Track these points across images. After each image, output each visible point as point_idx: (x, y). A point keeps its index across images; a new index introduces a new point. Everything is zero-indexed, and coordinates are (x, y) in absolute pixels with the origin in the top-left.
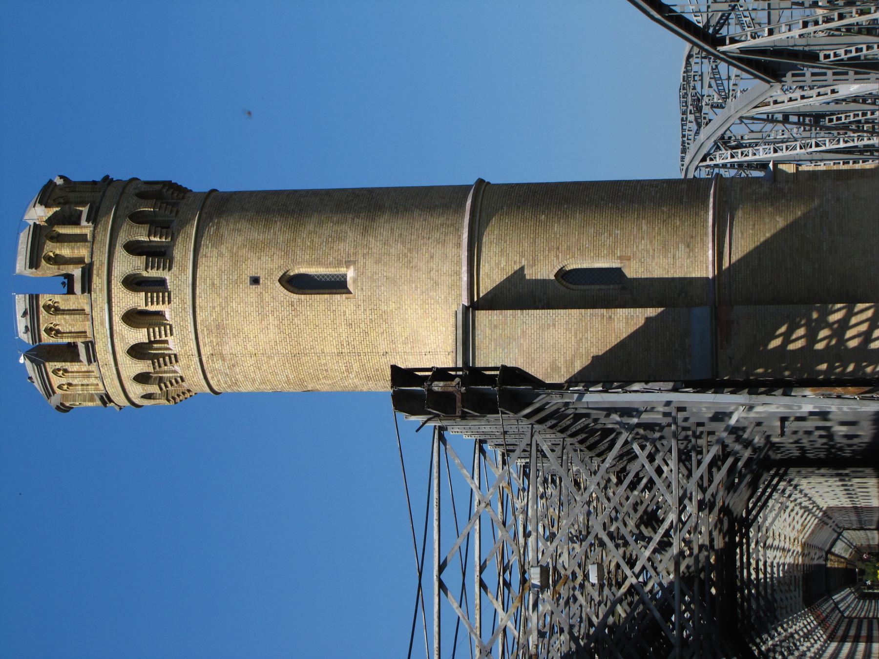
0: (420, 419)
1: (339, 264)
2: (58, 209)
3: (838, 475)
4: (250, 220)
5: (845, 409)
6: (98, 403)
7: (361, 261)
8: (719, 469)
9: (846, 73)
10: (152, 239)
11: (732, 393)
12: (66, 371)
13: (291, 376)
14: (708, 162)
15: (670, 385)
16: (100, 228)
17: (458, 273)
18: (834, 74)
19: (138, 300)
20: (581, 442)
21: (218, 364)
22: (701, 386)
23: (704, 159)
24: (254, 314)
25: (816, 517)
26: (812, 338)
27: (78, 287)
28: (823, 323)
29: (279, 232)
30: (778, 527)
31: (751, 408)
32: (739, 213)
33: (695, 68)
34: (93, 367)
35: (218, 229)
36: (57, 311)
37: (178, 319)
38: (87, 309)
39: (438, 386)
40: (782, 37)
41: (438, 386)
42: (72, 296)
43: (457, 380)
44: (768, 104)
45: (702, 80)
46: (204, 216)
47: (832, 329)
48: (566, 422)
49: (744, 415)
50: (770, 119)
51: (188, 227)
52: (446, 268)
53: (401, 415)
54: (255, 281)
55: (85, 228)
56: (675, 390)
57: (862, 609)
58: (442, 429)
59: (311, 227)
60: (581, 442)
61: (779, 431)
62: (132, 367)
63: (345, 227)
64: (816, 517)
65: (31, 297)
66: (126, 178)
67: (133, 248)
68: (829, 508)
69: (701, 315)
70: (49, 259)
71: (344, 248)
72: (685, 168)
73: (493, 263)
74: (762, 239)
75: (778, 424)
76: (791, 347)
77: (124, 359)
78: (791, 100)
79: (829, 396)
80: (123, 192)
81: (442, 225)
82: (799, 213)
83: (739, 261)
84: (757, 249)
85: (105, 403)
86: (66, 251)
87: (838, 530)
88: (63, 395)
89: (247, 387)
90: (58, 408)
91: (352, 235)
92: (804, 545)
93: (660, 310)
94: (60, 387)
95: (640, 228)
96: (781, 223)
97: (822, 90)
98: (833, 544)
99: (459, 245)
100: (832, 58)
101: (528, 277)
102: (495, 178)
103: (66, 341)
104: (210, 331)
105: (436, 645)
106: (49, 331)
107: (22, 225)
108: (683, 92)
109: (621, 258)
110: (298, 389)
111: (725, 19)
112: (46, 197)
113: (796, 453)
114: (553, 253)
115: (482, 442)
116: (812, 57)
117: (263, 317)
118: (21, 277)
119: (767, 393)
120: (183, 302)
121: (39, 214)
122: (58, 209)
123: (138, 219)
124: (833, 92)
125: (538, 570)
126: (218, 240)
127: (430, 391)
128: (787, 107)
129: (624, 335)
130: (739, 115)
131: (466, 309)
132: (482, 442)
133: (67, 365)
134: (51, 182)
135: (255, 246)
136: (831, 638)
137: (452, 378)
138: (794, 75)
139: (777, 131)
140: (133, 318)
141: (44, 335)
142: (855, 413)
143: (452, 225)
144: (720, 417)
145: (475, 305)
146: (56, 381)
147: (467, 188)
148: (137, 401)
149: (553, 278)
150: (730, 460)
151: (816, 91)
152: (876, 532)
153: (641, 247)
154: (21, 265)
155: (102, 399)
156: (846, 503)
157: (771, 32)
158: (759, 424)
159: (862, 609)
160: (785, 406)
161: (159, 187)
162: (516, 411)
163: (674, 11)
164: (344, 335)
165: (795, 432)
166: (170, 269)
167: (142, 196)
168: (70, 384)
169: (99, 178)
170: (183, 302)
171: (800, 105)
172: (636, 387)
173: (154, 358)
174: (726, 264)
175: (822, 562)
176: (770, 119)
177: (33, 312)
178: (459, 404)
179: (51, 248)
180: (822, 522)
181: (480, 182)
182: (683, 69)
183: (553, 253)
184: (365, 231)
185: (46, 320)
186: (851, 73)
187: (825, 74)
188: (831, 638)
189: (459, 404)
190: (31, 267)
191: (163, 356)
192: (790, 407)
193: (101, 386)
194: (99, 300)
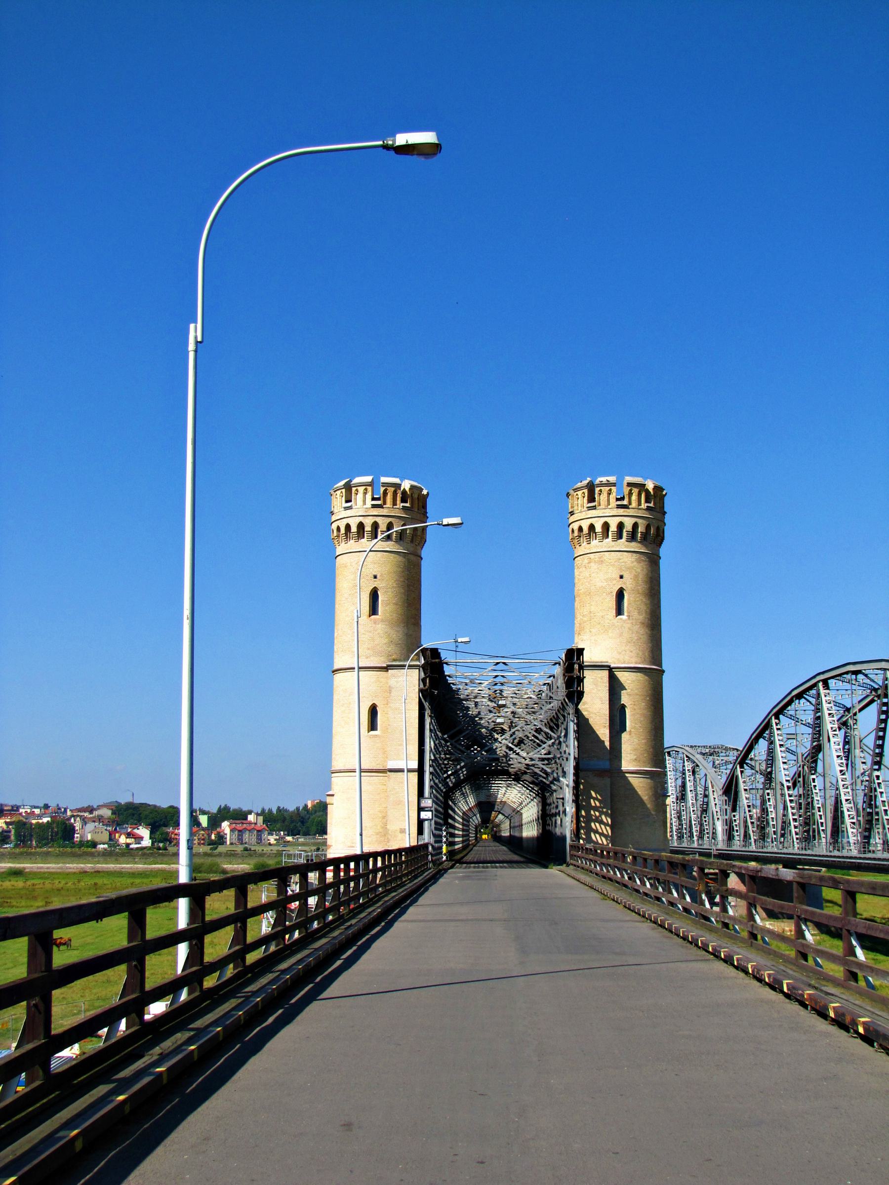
0: (564, 659)
1: (628, 612)
2: (652, 493)
3: (538, 818)
4: (647, 574)
5: (567, 824)
6: (571, 510)
7: (630, 622)
8: (540, 771)
9: (726, 825)
10: (639, 534)
11: (574, 780)
12: (584, 497)
13: (581, 591)
14: (686, 759)
15: (577, 756)
16: (644, 511)
17: (624, 663)
18: (726, 819)
19: (613, 528)
20: (553, 716)
21: (586, 561)
22: (576, 768)
23: (687, 756)
24: (607, 577)
25: (517, 808)
26: (596, 809)
27: (619, 503)
28: (601, 813)
29: (642, 587)
30: (515, 792)
31: (568, 786)
32: (649, 781)
33: (731, 753)
34: (585, 509)
35: (643, 561)
36: (609, 494)
37: (605, 544)
38: (609, 507)
39: (576, 667)
40: (743, 795)
41: (576, 667)
42: (615, 500)
43: (579, 674)
44: (713, 787)
45: (726, 756)
46: (649, 555)
47: (599, 816)
48: (561, 711)
49: (565, 784)
50: (706, 789)
51: (645, 548)
52: (627, 658)
53: (565, 651)
54: (621, 577)
55: (644, 505)
56: (575, 758)
57: (472, 827)
58: (559, 664)
59: (644, 600)
60: (553, 716)
61: (558, 797)
62: (585, 525)
63: (644, 615)
64: (517, 808)
65: (615, 483)
66: (665, 521)
67: (635, 526)
68: (521, 814)
69: (606, 765)
70: (631, 490)
71: (635, 614)
72: (683, 747)
73: (628, 677)
74: (638, 790)
75: (561, 797)
76: (592, 800)
77: (588, 522)
78: (714, 798)
79: (572, 818)
80: (659, 520)
81: (645, 656)
82: (649, 806)
83: (629, 781)
84: (634, 789)
85: (570, 513)
86: (634, 497)
87: (509, 817)
88: (573, 495)
89: (576, 572)
90: (568, 493)
91: (641, 618)
92: (505, 802)
93: (608, 748)
94: (577, 494)
95: (643, 739)
96: (645, 798)
97: (719, 814)
98: (503, 815)
99: (636, 663)
100: (733, 818)
101: (622, 692)
102: (665, 677)
103: (596, 496)
104: (600, 558)
105: (474, 661)
106: (601, 491)
107: (646, 479)
108: (720, 746)
109: (630, 731)
110: (575, 594)
111: (752, 768)
112: (658, 489)
113: (548, 801)
114: (633, 703)
115: (554, 677)
116: (734, 809)
117: (607, 580)
118: (624, 479)
119: (573, 794)
120: (613, 546)
121: (650, 486)
122: (652, 493)
123: (648, 527)
124: (718, 819)
125: (505, 703)
126: (638, 561)
127: (575, 663)
128: (711, 797)
129: (598, 733)
130: (708, 774)
131: (609, 666)
132: (554, 677)
133: (586, 498)
134: (664, 490)
135: (636, 577)
136: (464, 813)
137: (580, 672)
138: (726, 800)
139: (700, 790)
140: (606, 526)
141: (599, 489)
142: (566, 827)
143: (645, 660)
144: (564, 774)
145: (611, 670)
146: (580, 493)
147: (661, 666)
148: (571, 526)
149: (622, 703)
150: (545, 776)
151: (719, 811)
152: (509, 834)
153: (635, 740)
154: (629, 479)
155: (572, 512)
156: (524, 821)
157: (746, 790)
158: (561, 788)
159: (472, 827)
160: (568, 800)
161: (662, 535)
162: (567, 696)
163: (755, 745)
164: (598, 614)
165: (557, 802)
166: (627, 541)
167: (658, 529)
168: (578, 498)
169: (665, 510)
170: (613, 546)
171: (712, 803)
172: (576, 743)
173: (589, 534)
174: (627, 775)
175: (496, 809)
176: (706, 789)
177: (608, 484)
178: (569, 674)
179: (635, 491)
180: (514, 810)
181: (663, 671)
182: (732, 747)
183: (633, 703)
184: (642, 623)
185: (605, 489)
186: (726, 827)
187: (726, 815)
188: (464, 813)
189: (569, 674)
190: (628, 483)
191: (590, 538)
192: (568, 802)
193: (577, 512)
194: (613, 512)
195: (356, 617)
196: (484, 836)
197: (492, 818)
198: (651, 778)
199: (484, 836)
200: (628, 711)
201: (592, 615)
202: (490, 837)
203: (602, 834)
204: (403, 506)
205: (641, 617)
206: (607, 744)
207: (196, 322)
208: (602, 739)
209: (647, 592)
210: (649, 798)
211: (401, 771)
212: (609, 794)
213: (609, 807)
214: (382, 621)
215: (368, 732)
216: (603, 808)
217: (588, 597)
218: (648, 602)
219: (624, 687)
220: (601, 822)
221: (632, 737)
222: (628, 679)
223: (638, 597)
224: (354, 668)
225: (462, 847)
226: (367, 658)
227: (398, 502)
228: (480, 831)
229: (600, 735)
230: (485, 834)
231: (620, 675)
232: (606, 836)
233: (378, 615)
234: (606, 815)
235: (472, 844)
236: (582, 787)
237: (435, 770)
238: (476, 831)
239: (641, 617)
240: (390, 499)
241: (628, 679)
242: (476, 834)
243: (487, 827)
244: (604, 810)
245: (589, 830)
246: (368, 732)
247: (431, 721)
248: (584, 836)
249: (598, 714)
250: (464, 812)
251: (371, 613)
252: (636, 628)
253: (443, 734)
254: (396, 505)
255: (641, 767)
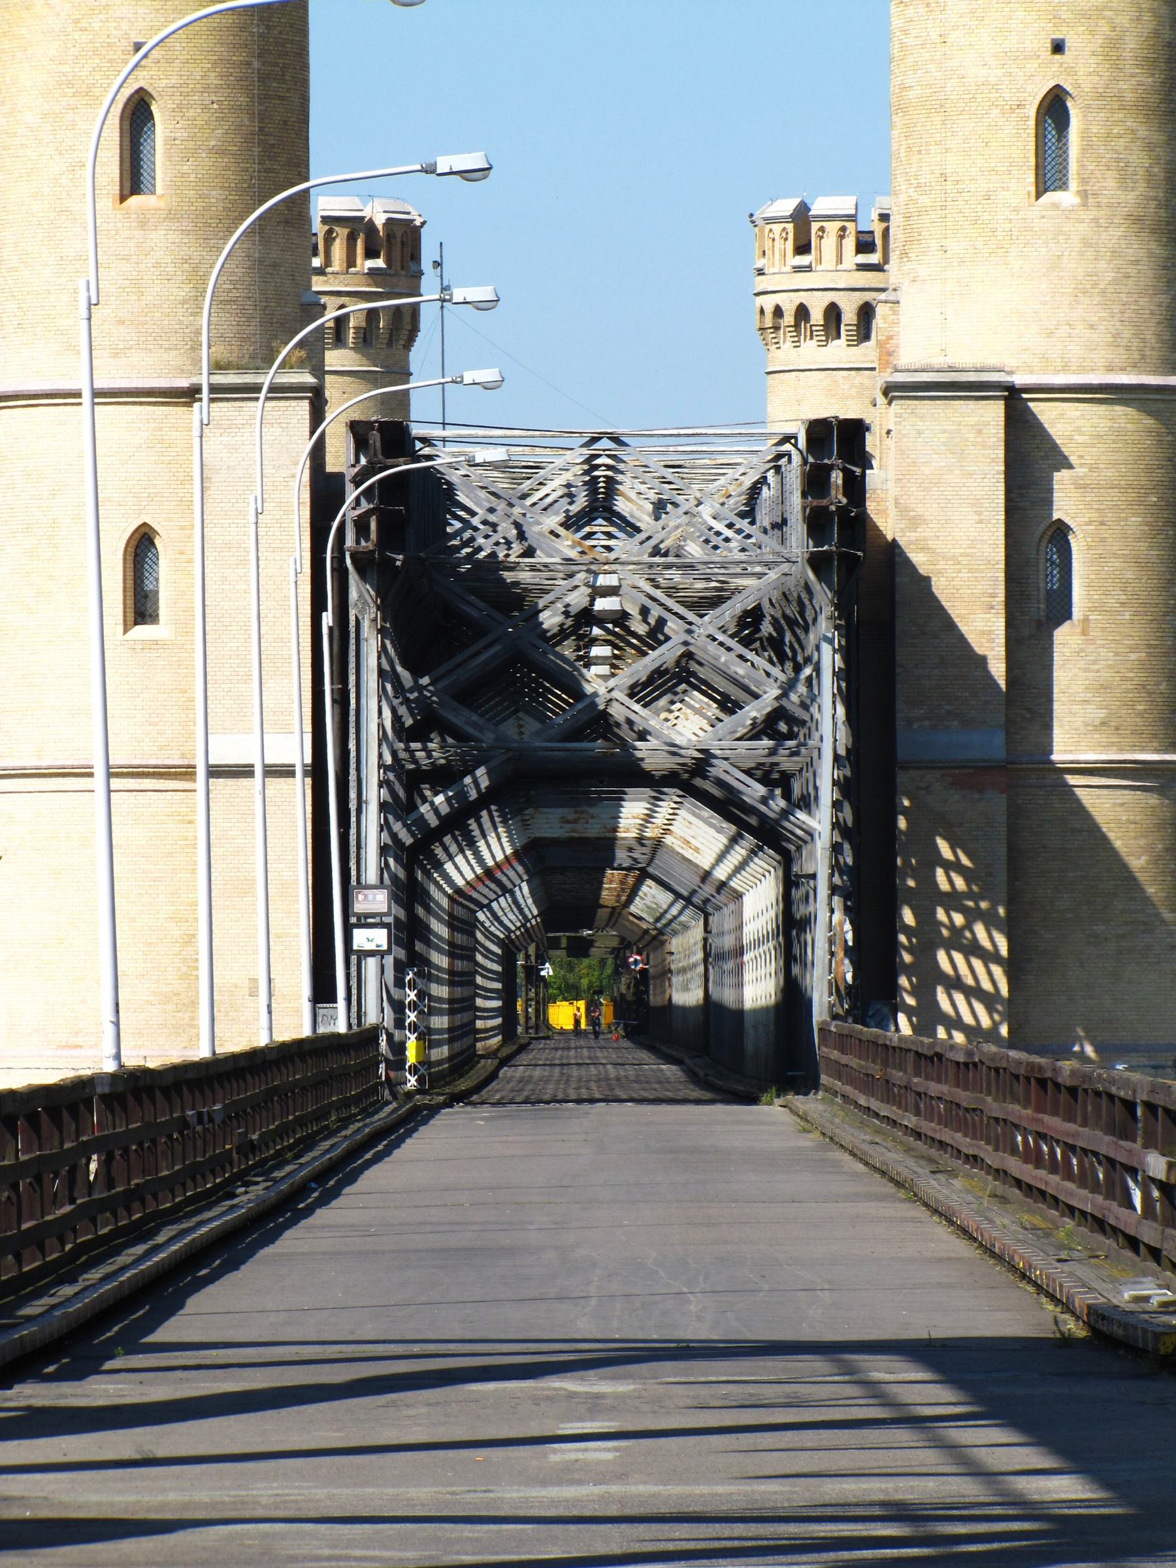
1: (1084, 181)
4: (1156, 33)
7: (1092, 214)
13: (911, 94)
17: (1065, 368)
26: (952, 901)
32: (1153, 800)
47: (964, 928)
54: (1058, 47)
59: (1143, 132)
62: (789, 304)
63: (1141, 187)
69: (995, 746)
71: (1108, 184)
73: (1080, 423)
74: (1111, 835)
81: (1144, 341)
82: (1151, 890)
83: (1078, 801)
93: (1002, 684)
94: (771, 230)
96: (1137, 862)
99: (1110, 369)
109: (1086, 620)
114: (1095, 516)
125: (615, 583)
129: (964, 628)
141: (819, 225)
143: (1143, 357)
149: (1056, 516)
172: (841, 710)
174: (1072, 780)
183: (1095, 516)
191: (798, 336)
195: (292, 573)
196: (563, 1015)
197: (894, 99)
198: (1161, 791)
199: (563, 1015)
200: (1077, 545)
201: (949, 186)
202: (607, 1014)
203: (973, 993)
204: (370, 269)
205: (1131, 196)
206: (998, 669)
207: (327, 611)
208: (979, 650)
209: (1154, 99)
210: (1156, 860)
211: (245, 771)
212: (1002, 851)
213: (1003, 895)
214: (171, 215)
215: (126, 631)
216: (976, 898)
217: (937, 119)
218: (1158, 138)
219: (1065, 458)
220: (973, 949)
221: (1091, 641)
222: (1078, 430)
223: (1117, 123)
224: (78, 395)
225: (451, 1058)
226: (116, 356)
227: (359, 260)
228: (532, 973)
229: (972, 639)
230: (570, 992)
231: (1046, 413)
232: (990, 1000)
233: (153, 193)
234: (990, 921)
235: (491, 1054)
236: (902, 823)
237: (393, 793)
238: (508, 976)
239: (1131, 196)
240: (341, 248)
241: (1078, 430)
242: (509, 995)
243: (580, 949)
244: (984, 905)
245: (928, 978)
246: (126, 631)
247: (383, 645)
248: (911, 1001)
249: (964, 561)
250: (458, 891)
251: (128, 184)
252: (1115, 236)
253: (416, 674)
254: (355, 266)
255: (1121, 750)
